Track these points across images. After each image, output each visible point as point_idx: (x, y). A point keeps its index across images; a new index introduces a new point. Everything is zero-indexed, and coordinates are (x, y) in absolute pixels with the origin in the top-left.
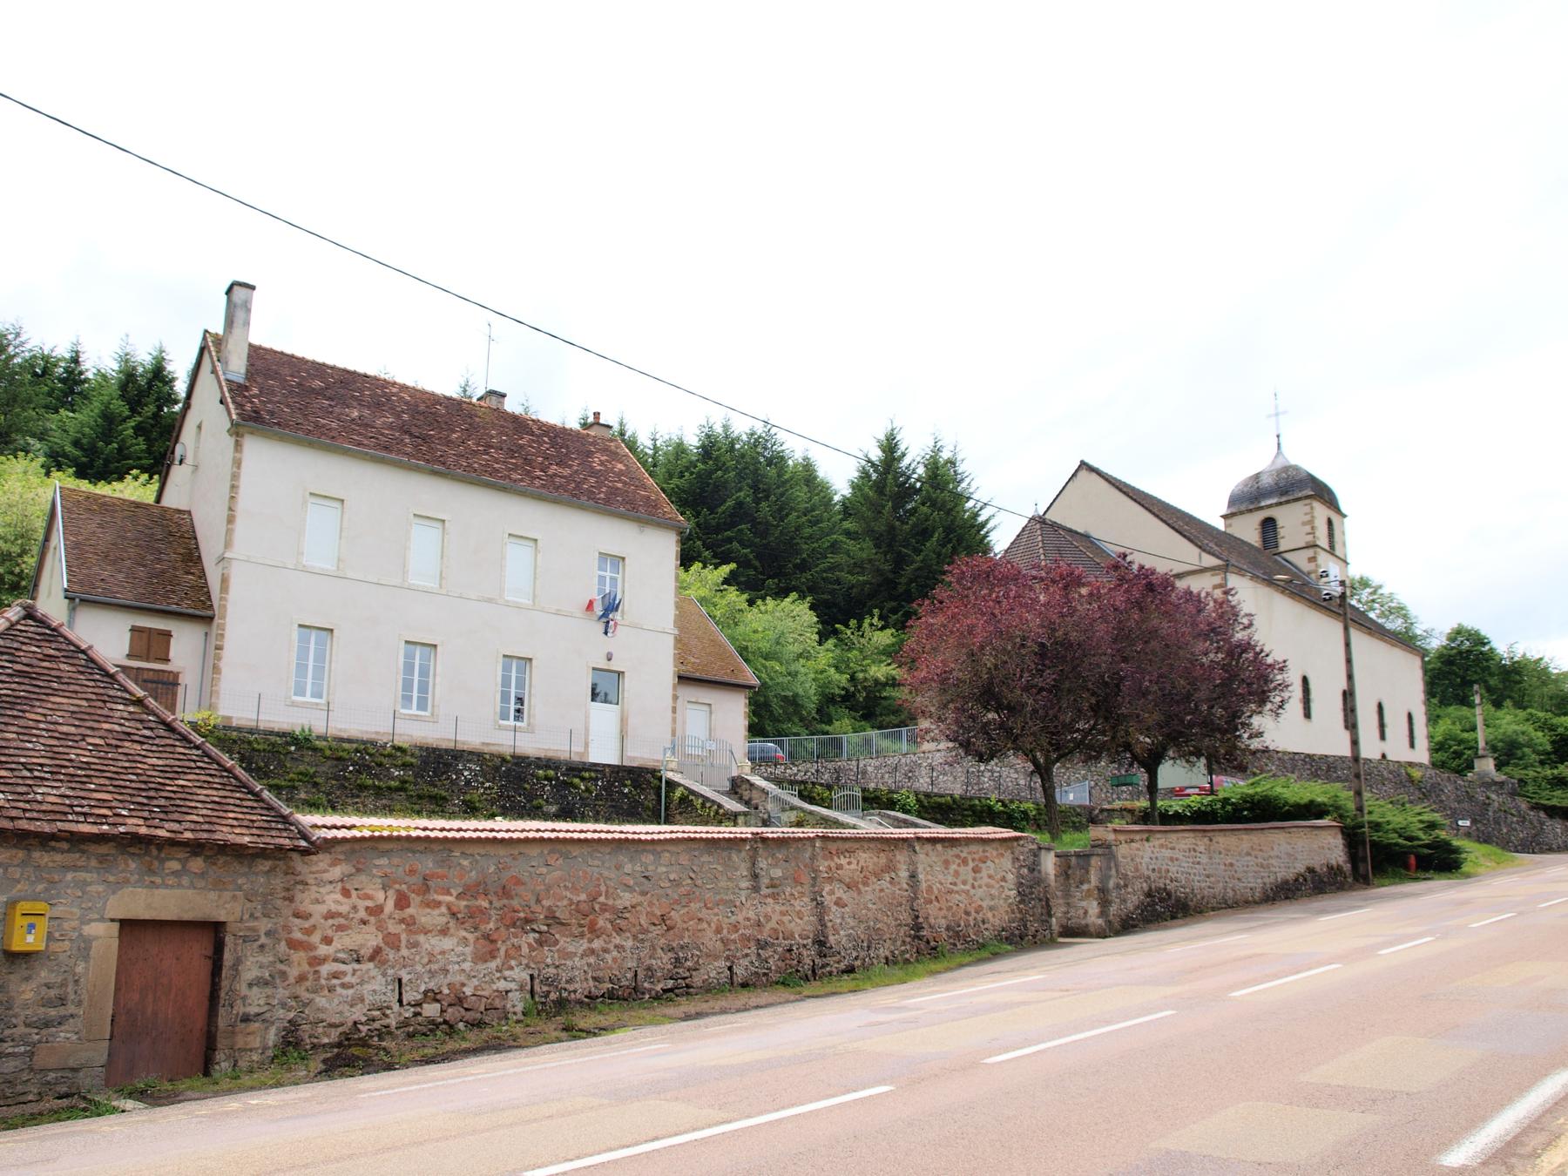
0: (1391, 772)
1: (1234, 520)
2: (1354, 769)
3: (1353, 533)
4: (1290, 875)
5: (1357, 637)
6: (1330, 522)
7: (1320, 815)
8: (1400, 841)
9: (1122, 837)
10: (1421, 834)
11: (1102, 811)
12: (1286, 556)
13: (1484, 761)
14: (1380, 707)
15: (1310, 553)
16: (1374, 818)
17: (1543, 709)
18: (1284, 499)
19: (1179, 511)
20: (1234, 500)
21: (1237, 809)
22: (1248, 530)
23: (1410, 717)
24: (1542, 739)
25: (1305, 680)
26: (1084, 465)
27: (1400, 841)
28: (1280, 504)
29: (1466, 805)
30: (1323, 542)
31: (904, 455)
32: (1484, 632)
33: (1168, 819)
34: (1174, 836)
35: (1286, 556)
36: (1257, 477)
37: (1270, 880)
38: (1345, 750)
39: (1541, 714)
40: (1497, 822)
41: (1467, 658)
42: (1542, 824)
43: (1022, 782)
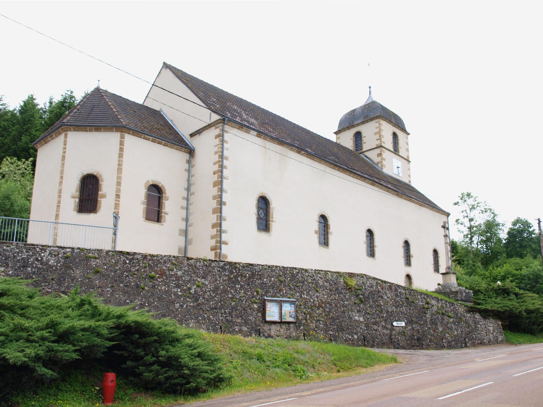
3: (412, 143)
12: (366, 154)
14: (407, 244)
15: (378, 151)
20: (341, 122)
23: (435, 252)
35: (366, 154)
42: (476, 323)
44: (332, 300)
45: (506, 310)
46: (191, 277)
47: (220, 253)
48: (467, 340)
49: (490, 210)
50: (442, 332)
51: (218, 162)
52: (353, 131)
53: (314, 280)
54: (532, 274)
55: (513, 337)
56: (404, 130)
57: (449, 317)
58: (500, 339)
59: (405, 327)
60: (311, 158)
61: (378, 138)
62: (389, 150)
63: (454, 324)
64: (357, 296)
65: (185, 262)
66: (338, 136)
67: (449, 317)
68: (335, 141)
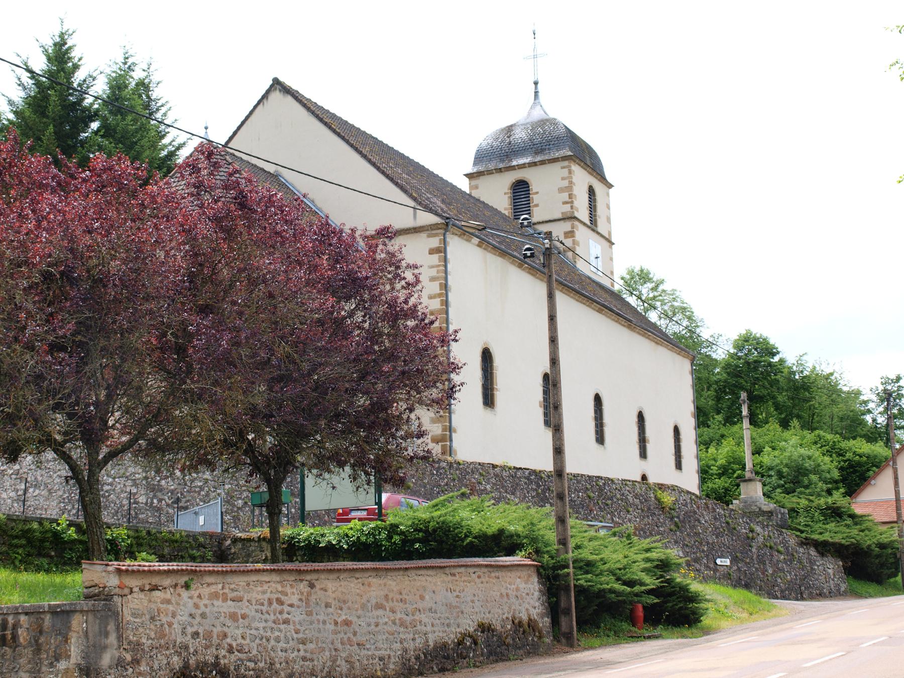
0: (636, 496)
1: (482, 181)
2: (551, 486)
3: (618, 206)
4: (450, 636)
5: (563, 301)
6: (591, 191)
7: (511, 550)
8: (617, 586)
9: (134, 582)
10: (647, 579)
11: (235, 540)
13: (751, 486)
14: (641, 417)
15: (567, 226)
16: (585, 554)
17: (833, 431)
18: (538, 158)
19: (397, 153)
20: (481, 157)
21: (407, 541)
22: (496, 194)
23: (676, 430)
24: (830, 466)
25: (487, 356)
26: (277, 85)
27: (617, 586)
28: (534, 164)
29: (726, 540)
30: (583, 214)
31: (76, 67)
32: (774, 340)
33: (315, 552)
34: (241, 580)
36: (509, 129)
37: (414, 644)
38: (546, 464)
39: (829, 437)
40: (762, 562)
41: (756, 369)
42: (812, 562)
43: (142, 499)
44: (645, 525)
45: (853, 544)
46: (500, 492)
47: (451, 447)
48: (803, 588)
49: (683, 310)
50: (772, 574)
51: (440, 295)
52: (511, 178)
53: (623, 494)
54: (787, 465)
55: (858, 586)
56: (602, 178)
57: (779, 552)
58: (843, 589)
59: (730, 567)
60: (532, 275)
61: (567, 199)
62: (585, 224)
63: (786, 563)
64: (672, 518)
65: (491, 471)
66: (474, 182)
67: (779, 552)
68: (468, 192)
